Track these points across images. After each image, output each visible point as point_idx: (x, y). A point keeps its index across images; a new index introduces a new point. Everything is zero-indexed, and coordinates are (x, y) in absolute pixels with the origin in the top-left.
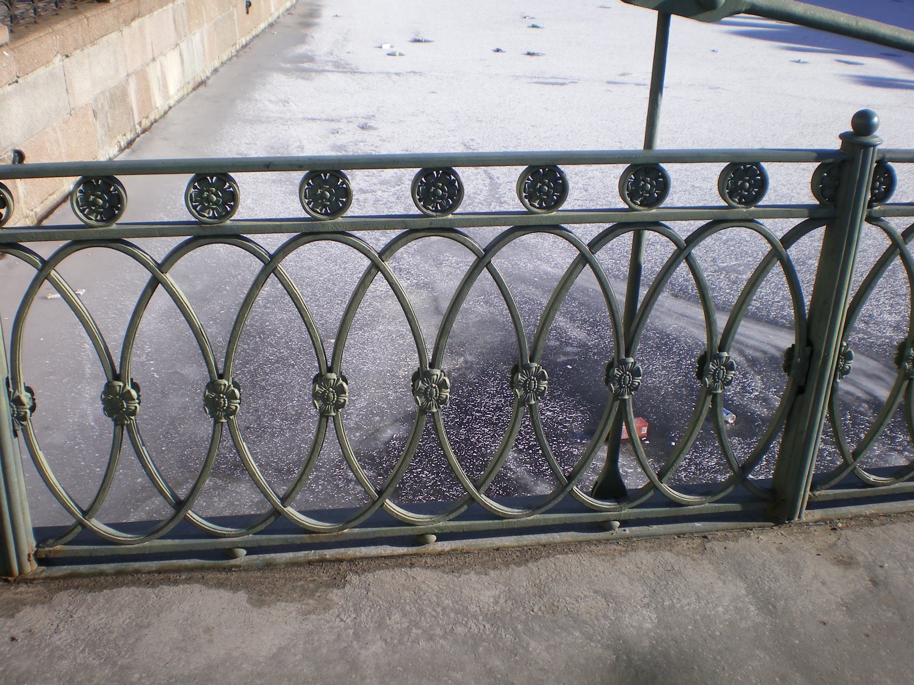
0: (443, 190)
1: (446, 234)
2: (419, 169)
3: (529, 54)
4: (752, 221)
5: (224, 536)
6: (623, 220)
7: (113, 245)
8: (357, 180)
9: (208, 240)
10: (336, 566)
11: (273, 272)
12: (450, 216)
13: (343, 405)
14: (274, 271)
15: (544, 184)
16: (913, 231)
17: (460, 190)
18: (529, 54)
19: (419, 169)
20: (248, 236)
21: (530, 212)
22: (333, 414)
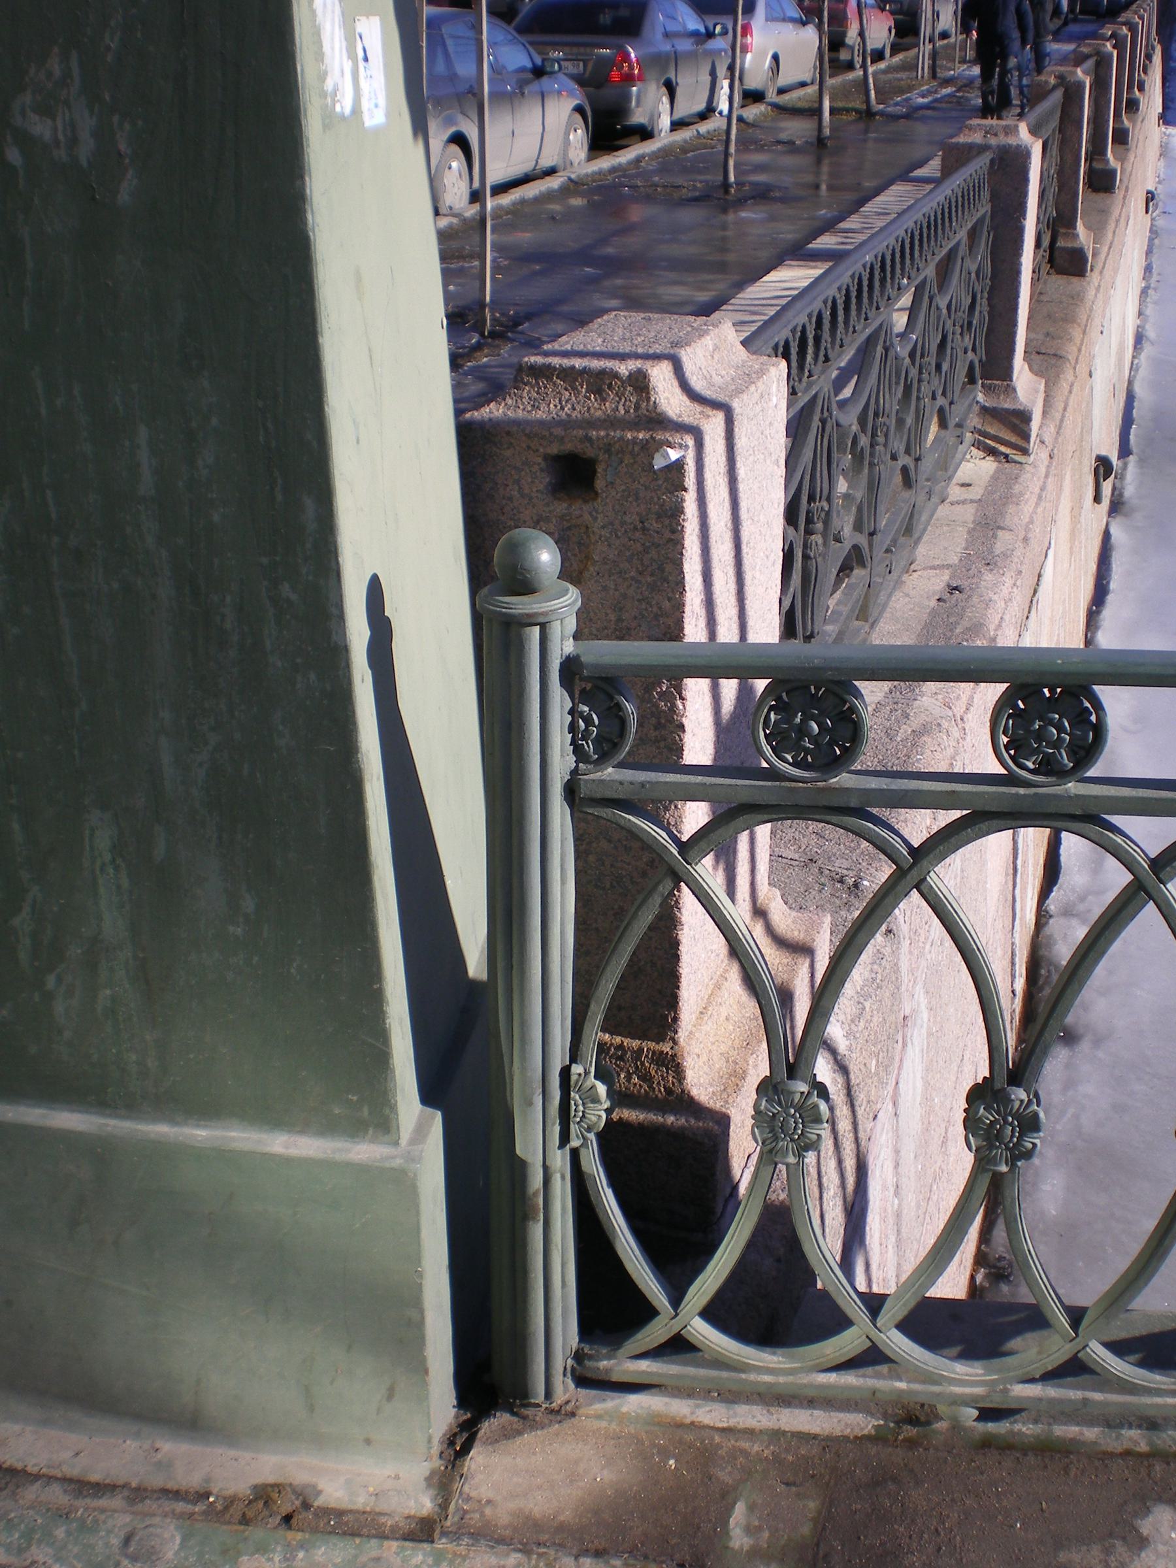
0: (1061, 729)
1: (835, 819)
2: (1006, 685)
3: (358, 442)
4: (861, 813)
5: (1148, 1391)
6: (745, 798)
7: (835, 819)
8: (1117, 703)
9: (995, 823)
10: (1146, 1463)
11: (917, 887)
12: (1072, 787)
13: (1028, 1155)
14: (920, 885)
15: (1051, 723)
16: (1175, 858)
17: (1099, 730)
18: (358, 442)
19: (1006, 685)
20: (875, 811)
21: (1009, 780)
22: (792, 1159)
